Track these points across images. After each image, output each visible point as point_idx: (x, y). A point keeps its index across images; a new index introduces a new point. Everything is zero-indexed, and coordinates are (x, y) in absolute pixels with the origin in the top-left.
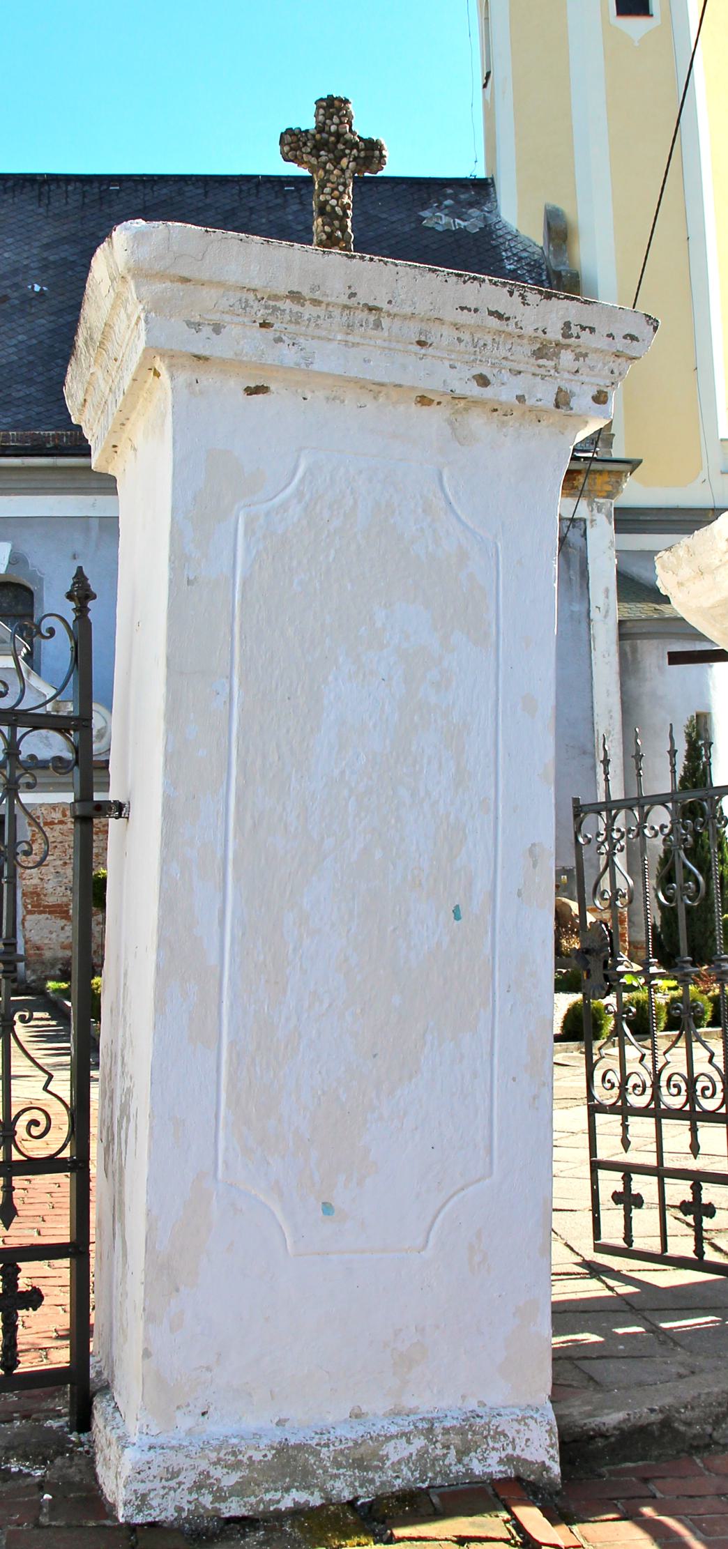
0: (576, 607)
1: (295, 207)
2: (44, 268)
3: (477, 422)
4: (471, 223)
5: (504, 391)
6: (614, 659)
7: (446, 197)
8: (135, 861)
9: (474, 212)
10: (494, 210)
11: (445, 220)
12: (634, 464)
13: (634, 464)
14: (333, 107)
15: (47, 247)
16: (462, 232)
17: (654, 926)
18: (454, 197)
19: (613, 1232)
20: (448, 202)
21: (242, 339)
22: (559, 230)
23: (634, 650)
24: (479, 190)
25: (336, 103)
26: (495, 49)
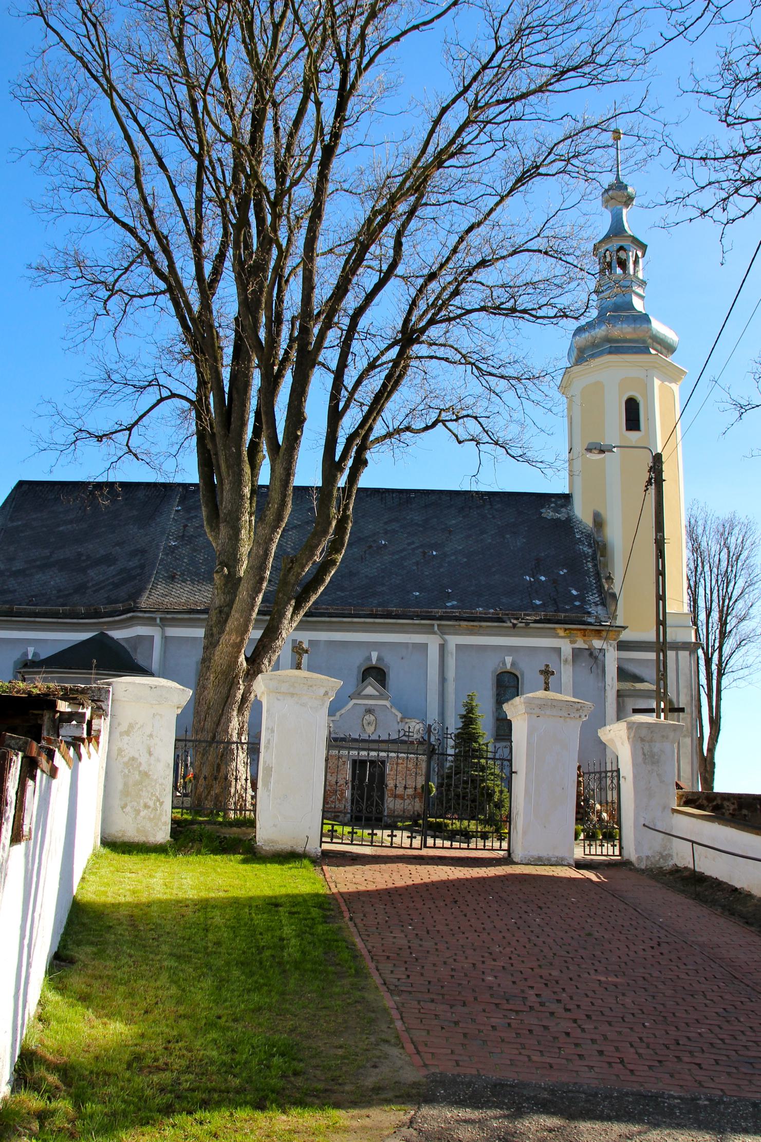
0: (600, 684)
1: (489, 507)
2: (386, 533)
3: (568, 720)
4: (562, 516)
5: (572, 716)
6: (615, 706)
7: (552, 502)
8: (519, 783)
9: (563, 510)
10: (572, 509)
11: (551, 514)
12: (624, 628)
13: (624, 628)
14: (547, 666)
15: (386, 523)
16: (559, 519)
17: (297, 609)
18: (555, 503)
19: (587, 852)
20: (553, 505)
21: (537, 711)
22: (599, 522)
23: (623, 702)
24: (566, 499)
25: (579, 816)
26: (574, 423)
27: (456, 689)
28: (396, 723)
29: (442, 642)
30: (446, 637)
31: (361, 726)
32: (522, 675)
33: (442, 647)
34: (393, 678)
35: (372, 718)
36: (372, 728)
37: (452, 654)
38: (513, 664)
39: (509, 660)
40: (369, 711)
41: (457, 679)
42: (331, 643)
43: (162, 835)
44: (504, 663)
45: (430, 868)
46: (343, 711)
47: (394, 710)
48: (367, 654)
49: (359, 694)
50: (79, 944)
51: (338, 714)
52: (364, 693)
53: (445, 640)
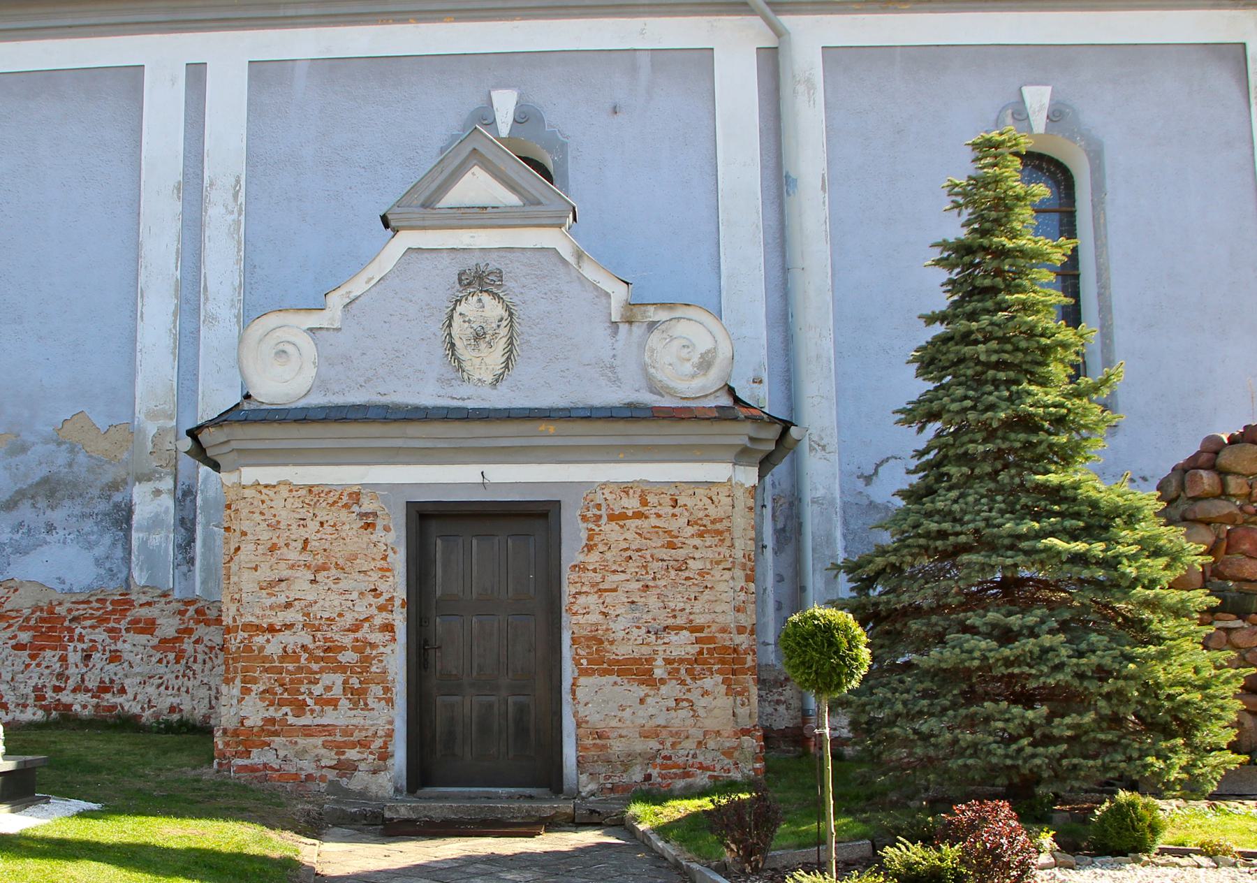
27: (835, 221)
28: (602, 332)
29: (769, 41)
30: (786, 21)
31: (440, 350)
32: (1096, 156)
33: (772, 63)
34: (581, 181)
35: (493, 310)
36: (494, 358)
37: (810, 84)
38: (1056, 116)
39: (1038, 99)
40: (478, 280)
41: (830, 183)
42: (332, 67)
43: (386, 780)
44: (1020, 113)
45: (501, 404)
46: (358, 287)
47: (590, 272)
48: (476, 101)
49: (427, 204)
50: (579, 792)
51: (336, 300)
52: (453, 198)
53: (779, 32)
